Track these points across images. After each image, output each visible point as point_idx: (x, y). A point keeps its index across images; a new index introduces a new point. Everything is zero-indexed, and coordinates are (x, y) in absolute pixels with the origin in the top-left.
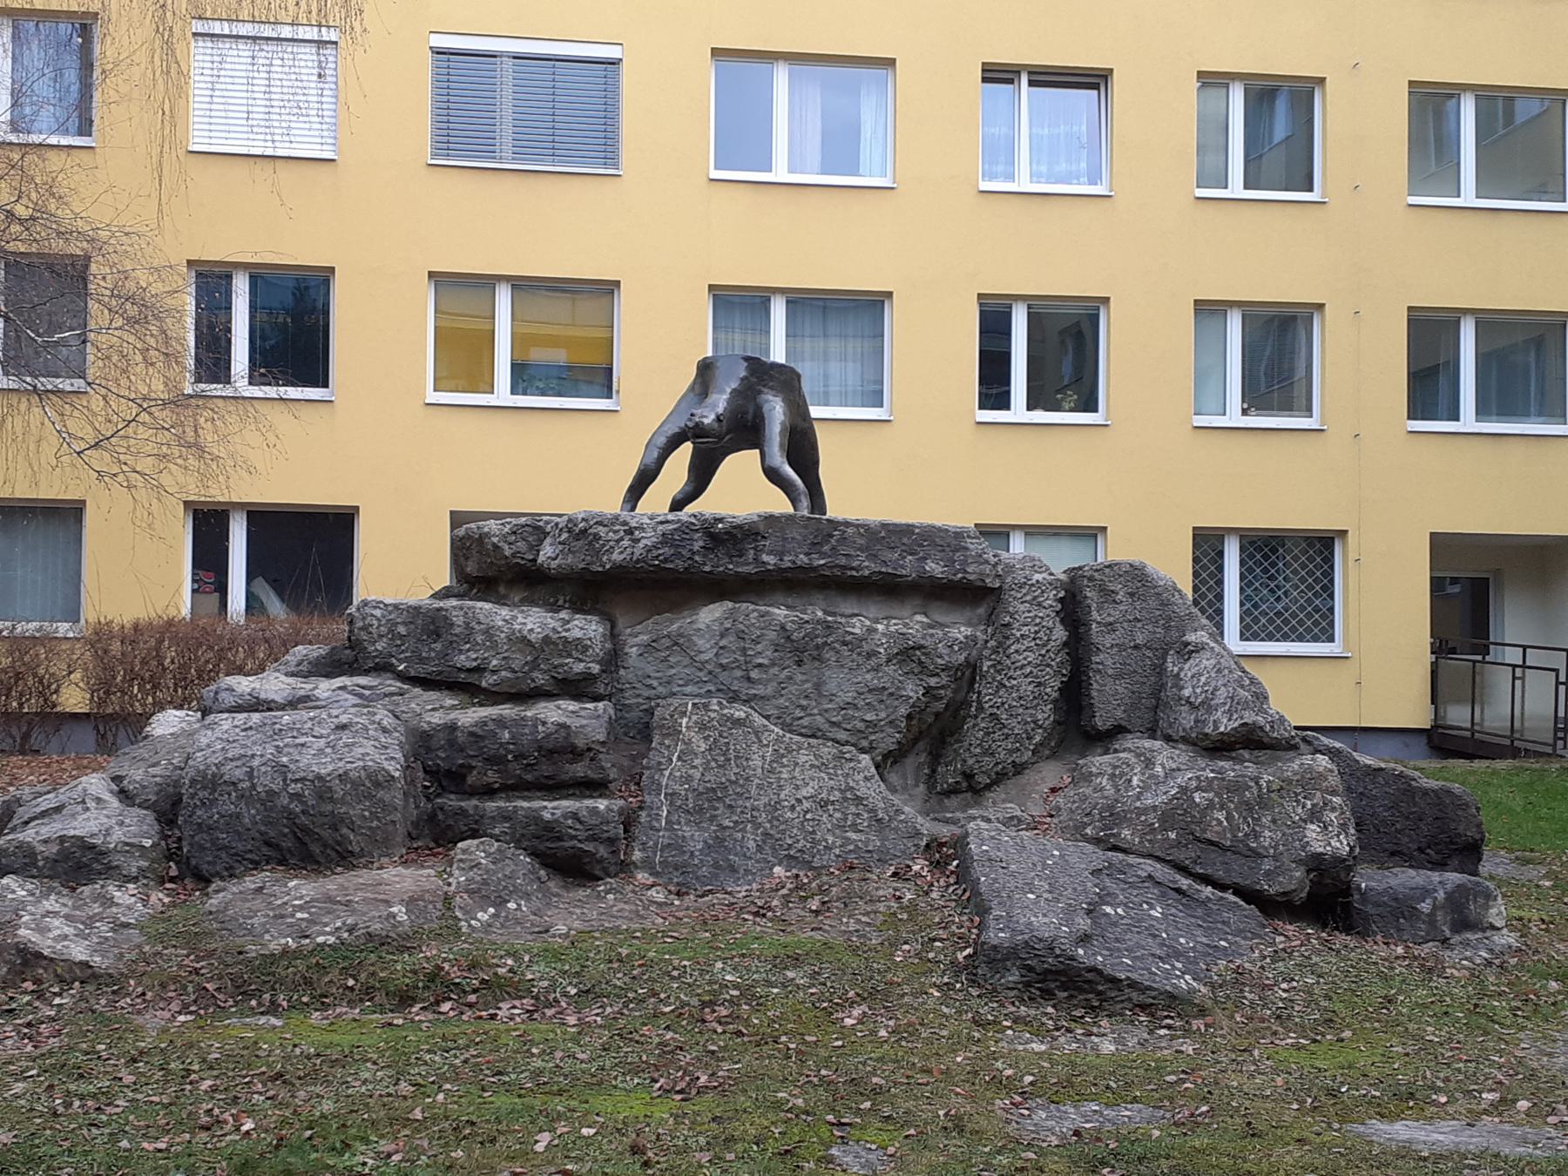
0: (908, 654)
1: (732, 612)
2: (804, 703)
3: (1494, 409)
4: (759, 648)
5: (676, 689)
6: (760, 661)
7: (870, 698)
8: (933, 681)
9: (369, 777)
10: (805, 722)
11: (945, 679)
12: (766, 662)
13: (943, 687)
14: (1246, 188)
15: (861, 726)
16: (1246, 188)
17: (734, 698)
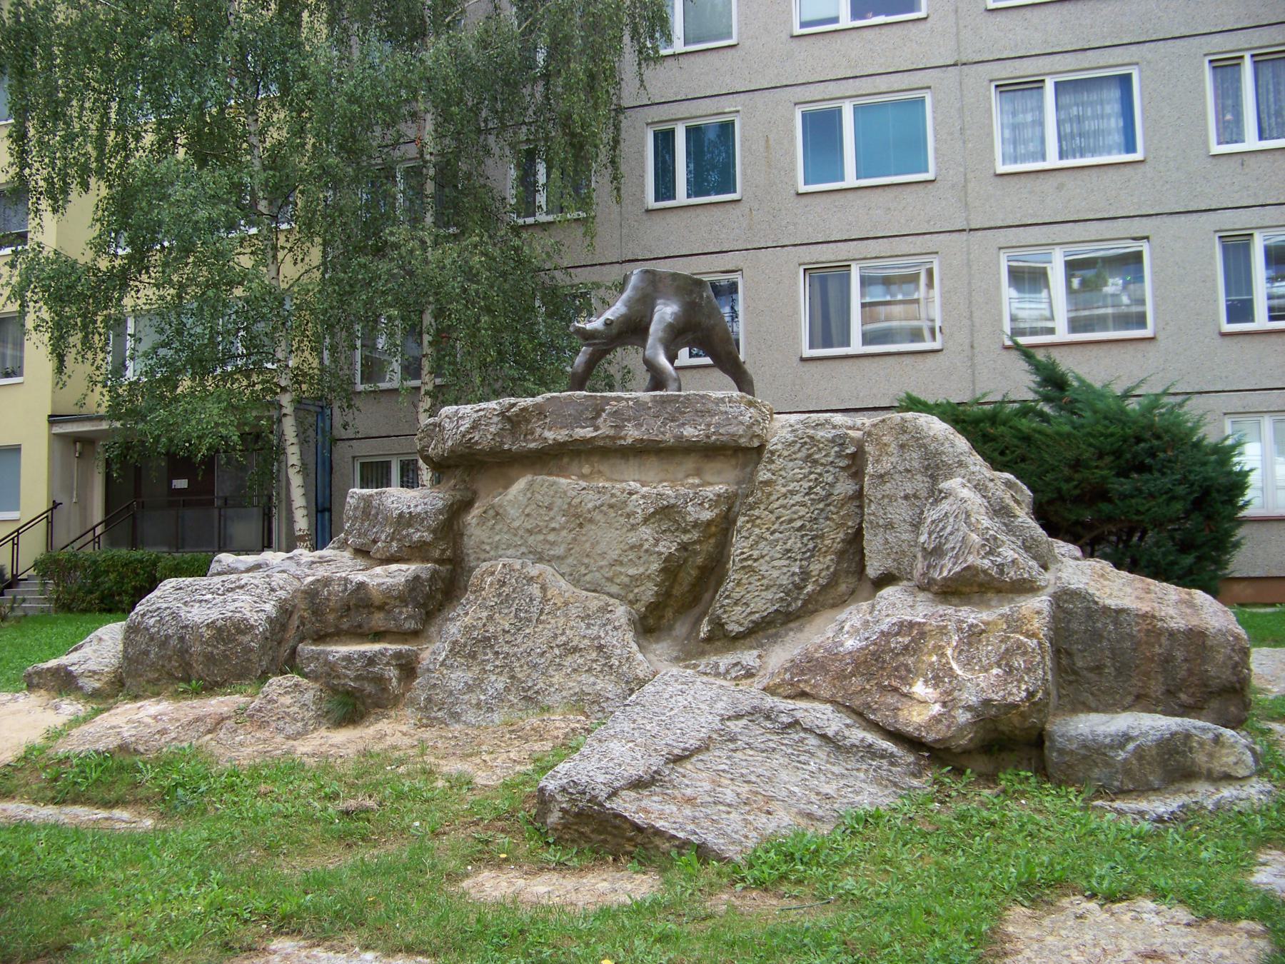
0: (665, 513)
1: (531, 484)
2: (586, 561)
3: (1073, 314)
4: (552, 514)
5: (501, 552)
6: (553, 525)
7: (632, 555)
8: (686, 538)
9: (233, 624)
10: (588, 578)
11: (695, 535)
12: (557, 526)
13: (695, 543)
14: (858, 178)
15: (627, 580)
16: (858, 178)
17: (540, 559)
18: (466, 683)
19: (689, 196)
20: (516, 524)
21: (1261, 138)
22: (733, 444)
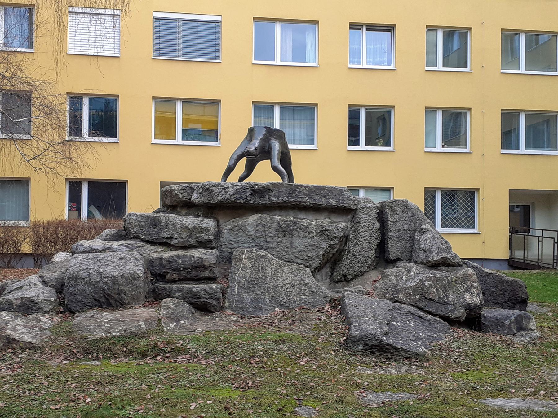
0: (323, 233)
1: (260, 217)
2: (286, 250)
4: (270, 230)
6: (270, 235)
7: (310, 248)
8: (332, 242)
10: (286, 257)
12: (273, 235)
15: (306, 258)
17: (261, 248)
18: (251, 299)
19: (443, 146)
20: (251, 234)
21: (281, 61)
22: (348, 207)
